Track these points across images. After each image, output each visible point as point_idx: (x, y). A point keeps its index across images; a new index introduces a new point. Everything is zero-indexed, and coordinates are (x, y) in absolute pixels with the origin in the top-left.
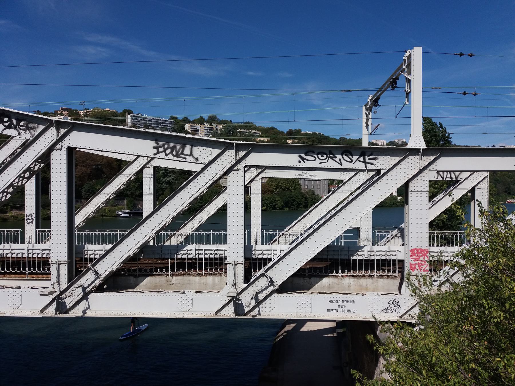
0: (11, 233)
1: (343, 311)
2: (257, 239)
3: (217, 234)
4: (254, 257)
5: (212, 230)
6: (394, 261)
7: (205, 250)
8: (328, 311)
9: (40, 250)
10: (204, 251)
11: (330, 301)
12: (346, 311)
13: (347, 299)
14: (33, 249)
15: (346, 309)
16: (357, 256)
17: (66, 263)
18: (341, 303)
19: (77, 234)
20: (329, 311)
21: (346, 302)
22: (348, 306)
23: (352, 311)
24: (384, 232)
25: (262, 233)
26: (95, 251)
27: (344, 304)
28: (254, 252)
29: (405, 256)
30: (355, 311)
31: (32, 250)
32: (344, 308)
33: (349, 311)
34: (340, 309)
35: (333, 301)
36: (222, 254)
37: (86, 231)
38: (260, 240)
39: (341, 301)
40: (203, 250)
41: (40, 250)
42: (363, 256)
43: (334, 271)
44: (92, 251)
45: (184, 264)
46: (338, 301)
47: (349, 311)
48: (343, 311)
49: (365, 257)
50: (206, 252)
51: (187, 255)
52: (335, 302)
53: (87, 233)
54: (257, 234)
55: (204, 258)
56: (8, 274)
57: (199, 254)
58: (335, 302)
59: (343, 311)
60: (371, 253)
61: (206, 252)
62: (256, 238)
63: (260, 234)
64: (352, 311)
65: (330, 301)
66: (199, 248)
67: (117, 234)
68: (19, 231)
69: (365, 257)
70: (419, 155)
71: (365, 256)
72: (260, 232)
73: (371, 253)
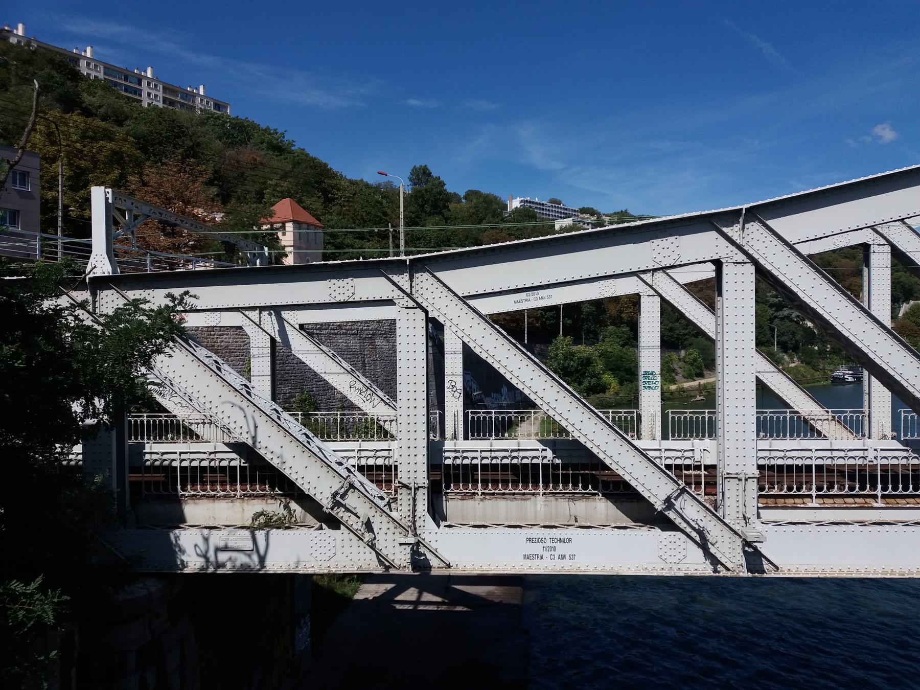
0: (160, 421)
1: (552, 558)
2: (456, 427)
3: (503, 418)
4: (448, 462)
5: (707, 411)
6: (809, 468)
7: (181, 453)
8: (525, 558)
9: (204, 453)
10: (180, 455)
11: (529, 540)
12: (557, 557)
13: (559, 537)
14: (491, 451)
15: (557, 554)
16: (683, 459)
17: (756, 478)
18: (549, 544)
19: (493, 417)
20: (526, 557)
21: (556, 540)
22: (561, 548)
23: (568, 557)
24: (625, 413)
25: (466, 416)
26: (163, 454)
27: (553, 545)
28: (147, 457)
29: (718, 456)
30: (572, 557)
31: (862, 452)
32: (553, 553)
33: (562, 557)
34: (546, 554)
35: (534, 539)
36: (477, 458)
37: (161, 416)
38: (462, 429)
39: (548, 540)
40: (178, 453)
41: (204, 453)
42: (693, 459)
43: (590, 486)
44: (157, 453)
45: (905, 477)
46: (543, 540)
47: (562, 557)
48: (552, 557)
49: (696, 462)
50: (183, 456)
51: (188, 461)
52: (538, 541)
53: (688, 416)
54: (456, 417)
55: (481, 464)
56: (909, 498)
57: (483, 458)
58: (538, 541)
59: (552, 557)
60: (770, 454)
61: (183, 456)
62: (455, 425)
63: (461, 418)
64: (568, 557)
65: (529, 540)
66: (215, 449)
67: (786, 417)
68: (635, 414)
69: (696, 462)
70: (739, 223)
71: (696, 460)
72: (461, 414)
73: (770, 454)
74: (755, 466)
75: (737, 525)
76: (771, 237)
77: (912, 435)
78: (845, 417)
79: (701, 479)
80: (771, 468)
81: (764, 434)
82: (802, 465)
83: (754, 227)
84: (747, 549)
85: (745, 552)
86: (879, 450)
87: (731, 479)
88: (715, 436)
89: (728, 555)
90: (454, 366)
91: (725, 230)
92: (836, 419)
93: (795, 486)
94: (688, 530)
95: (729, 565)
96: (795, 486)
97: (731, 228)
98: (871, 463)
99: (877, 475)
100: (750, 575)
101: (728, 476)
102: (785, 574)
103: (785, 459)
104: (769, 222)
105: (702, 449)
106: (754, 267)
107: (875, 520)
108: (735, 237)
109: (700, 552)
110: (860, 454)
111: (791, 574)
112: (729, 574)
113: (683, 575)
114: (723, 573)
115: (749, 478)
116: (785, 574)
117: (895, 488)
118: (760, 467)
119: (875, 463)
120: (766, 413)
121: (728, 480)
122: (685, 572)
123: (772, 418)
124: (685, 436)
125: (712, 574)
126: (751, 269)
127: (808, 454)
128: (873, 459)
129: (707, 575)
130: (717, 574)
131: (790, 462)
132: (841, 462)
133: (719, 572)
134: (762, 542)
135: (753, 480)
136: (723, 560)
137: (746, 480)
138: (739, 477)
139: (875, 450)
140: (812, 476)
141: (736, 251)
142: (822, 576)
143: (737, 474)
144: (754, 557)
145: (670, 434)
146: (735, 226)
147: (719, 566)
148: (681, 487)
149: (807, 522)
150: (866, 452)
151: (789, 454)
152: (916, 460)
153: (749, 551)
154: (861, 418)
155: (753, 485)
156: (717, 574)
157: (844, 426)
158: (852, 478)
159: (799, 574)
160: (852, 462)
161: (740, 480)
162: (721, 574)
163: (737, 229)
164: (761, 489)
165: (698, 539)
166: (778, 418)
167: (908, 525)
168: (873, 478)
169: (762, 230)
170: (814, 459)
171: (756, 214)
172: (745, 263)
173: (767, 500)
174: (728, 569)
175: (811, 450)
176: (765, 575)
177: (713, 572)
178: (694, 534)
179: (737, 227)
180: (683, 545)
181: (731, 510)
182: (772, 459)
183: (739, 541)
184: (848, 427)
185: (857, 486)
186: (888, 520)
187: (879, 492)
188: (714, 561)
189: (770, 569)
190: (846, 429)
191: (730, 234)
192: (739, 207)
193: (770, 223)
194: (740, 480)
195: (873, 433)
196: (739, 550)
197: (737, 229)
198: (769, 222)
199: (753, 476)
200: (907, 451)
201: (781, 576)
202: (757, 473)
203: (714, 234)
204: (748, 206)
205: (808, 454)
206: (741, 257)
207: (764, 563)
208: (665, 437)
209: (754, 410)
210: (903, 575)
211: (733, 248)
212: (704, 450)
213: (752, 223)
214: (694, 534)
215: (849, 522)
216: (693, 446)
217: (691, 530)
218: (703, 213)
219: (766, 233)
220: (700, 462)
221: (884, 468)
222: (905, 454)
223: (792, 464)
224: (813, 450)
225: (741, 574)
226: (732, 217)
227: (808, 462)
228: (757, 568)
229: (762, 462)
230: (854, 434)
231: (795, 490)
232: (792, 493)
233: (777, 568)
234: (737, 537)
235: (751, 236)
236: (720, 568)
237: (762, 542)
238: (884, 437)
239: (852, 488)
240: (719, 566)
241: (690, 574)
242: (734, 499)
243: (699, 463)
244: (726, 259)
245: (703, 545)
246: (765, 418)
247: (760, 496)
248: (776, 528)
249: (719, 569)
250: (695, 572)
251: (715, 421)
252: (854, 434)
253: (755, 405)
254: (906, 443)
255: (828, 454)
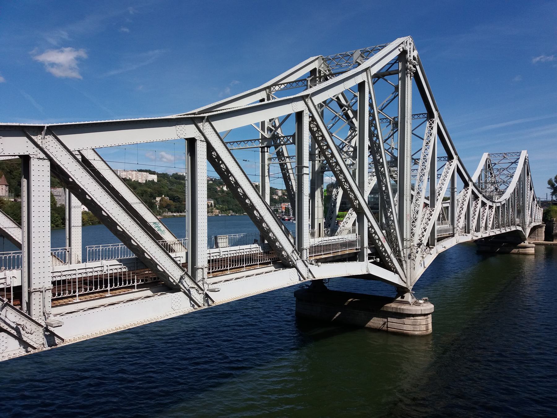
17: (50, 289)
42: (5, 284)
49: (7, 285)
60: (53, 275)
69: (7, 285)
70: (41, 134)
71: (8, 284)
73: (53, 275)
74: (51, 282)
75: (40, 320)
76: (59, 146)
77: (127, 256)
78: (58, 253)
79: (11, 296)
80: (59, 282)
81: (4, 268)
82: (71, 279)
83: (50, 138)
84: (46, 333)
85: (45, 335)
86: (108, 266)
87: (36, 292)
88: (21, 267)
89: (34, 340)
90: (25, 224)
91: (33, 137)
92: (53, 254)
93: (57, 293)
94: (9, 329)
95: (35, 346)
96: (57, 293)
97: (36, 137)
98: (105, 273)
99: (108, 279)
100: (49, 348)
101: (34, 291)
102: (69, 342)
103: (62, 276)
104: (59, 137)
105: (12, 276)
106: (49, 162)
107: (128, 299)
108: (39, 143)
109: (17, 342)
110: (100, 269)
111: (72, 342)
112: (37, 351)
113: (8, 359)
114: (32, 351)
115: (47, 290)
116: (69, 342)
117: (116, 285)
118: (53, 283)
119: (107, 273)
120: (10, 253)
121: (34, 293)
122: (8, 357)
123: (14, 256)
124: (112, 258)
125: (26, 354)
126: (48, 163)
127: (74, 272)
128: (106, 271)
129: (23, 355)
130: (29, 353)
131: (64, 278)
132: (90, 274)
133: (30, 352)
134: (61, 326)
135: (49, 291)
136: (31, 344)
137: (45, 291)
138: (41, 290)
139: (107, 266)
140: (11, 294)
141: (39, 151)
142: (88, 339)
143: (40, 288)
144: (50, 337)
145: (88, 260)
146: (38, 136)
147: (29, 348)
148: (5, 302)
149: (76, 311)
150: (102, 268)
151: (64, 273)
152: (125, 269)
153: (47, 334)
154: (20, 257)
155: (49, 295)
156: (29, 353)
157: (57, 258)
158: (86, 284)
159: (76, 340)
160: (96, 274)
161: (42, 292)
162: (32, 352)
163: (40, 138)
164: (54, 295)
165: (15, 334)
166: (115, 248)
167: (85, 311)
168: (106, 280)
169: (55, 141)
170: (77, 274)
171: (54, 131)
172: (44, 159)
173: (56, 301)
174: (35, 348)
175: (75, 270)
176: (58, 346)
177: (26, 352)
178: (13, 332)
179: (39, 137)
180: (6, 341)
181: (36, 313)
182: (54, 278)
183: (41, 329)
184: (59, 258)
185: (94, 287)
186: (94, 306)
187: (109, 288)
188: (25, 345)
189: (60, 342)
190: (59, 259)
191: (36, 140)
192: (42, 125)
193: (60, 137)
194: (42, 292)
195: (72, 261)
196: (42, 335)
197: (40, 138)
198: (59, 137)
199: (49, 288)
200: (121, 265)
201: (67, 344)
202: (51, 286)
203: (25, 139)
204: (48, 125)
205: (74, 272)
206: (42, 155)
207: (56, 339)
208: (84, 260)
209: (50, 249)
210: (125, 328)
211: (37, 149)
212: (13, 277)
213: (49, 136)
214: (13, 332)
215: (97, 306)
216: (5, 276)
217: (10, 329)
218: (21, 125)
219: (57, 143)
220: (10, 285)
221: (111, 275)
222: (120, 267)
223: (3, 287)
224: (77, 270)
225: (44, 349)
226: (38, 130)
227: (74, 277)
228: (52, 343)
229: (54, 279)
230: (63, 262)
231: (57, 295)
232: (121, 286)
233: (63, 340)
234: (40, 327)
235: (48, 143)
236: (30, 349)
237: (61, 326)
238: (79, 262)
239: (91, 289)
240: (29, 348)
241: (12, 358)
242: (38, 304)
243: (9, 286)
244: (33, 156)
245: (19, 338)
246: (10, 257)
247: (53, 300)
248: (85, 312)
249: (29, 350)
250: (15, 355)
251: (21, 258)
252: (63, 262)
253: (50, 245)
254: (120, 261)
255: (84, 271)
